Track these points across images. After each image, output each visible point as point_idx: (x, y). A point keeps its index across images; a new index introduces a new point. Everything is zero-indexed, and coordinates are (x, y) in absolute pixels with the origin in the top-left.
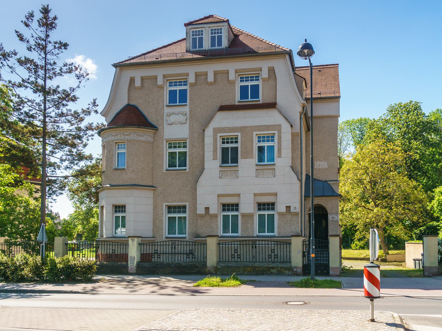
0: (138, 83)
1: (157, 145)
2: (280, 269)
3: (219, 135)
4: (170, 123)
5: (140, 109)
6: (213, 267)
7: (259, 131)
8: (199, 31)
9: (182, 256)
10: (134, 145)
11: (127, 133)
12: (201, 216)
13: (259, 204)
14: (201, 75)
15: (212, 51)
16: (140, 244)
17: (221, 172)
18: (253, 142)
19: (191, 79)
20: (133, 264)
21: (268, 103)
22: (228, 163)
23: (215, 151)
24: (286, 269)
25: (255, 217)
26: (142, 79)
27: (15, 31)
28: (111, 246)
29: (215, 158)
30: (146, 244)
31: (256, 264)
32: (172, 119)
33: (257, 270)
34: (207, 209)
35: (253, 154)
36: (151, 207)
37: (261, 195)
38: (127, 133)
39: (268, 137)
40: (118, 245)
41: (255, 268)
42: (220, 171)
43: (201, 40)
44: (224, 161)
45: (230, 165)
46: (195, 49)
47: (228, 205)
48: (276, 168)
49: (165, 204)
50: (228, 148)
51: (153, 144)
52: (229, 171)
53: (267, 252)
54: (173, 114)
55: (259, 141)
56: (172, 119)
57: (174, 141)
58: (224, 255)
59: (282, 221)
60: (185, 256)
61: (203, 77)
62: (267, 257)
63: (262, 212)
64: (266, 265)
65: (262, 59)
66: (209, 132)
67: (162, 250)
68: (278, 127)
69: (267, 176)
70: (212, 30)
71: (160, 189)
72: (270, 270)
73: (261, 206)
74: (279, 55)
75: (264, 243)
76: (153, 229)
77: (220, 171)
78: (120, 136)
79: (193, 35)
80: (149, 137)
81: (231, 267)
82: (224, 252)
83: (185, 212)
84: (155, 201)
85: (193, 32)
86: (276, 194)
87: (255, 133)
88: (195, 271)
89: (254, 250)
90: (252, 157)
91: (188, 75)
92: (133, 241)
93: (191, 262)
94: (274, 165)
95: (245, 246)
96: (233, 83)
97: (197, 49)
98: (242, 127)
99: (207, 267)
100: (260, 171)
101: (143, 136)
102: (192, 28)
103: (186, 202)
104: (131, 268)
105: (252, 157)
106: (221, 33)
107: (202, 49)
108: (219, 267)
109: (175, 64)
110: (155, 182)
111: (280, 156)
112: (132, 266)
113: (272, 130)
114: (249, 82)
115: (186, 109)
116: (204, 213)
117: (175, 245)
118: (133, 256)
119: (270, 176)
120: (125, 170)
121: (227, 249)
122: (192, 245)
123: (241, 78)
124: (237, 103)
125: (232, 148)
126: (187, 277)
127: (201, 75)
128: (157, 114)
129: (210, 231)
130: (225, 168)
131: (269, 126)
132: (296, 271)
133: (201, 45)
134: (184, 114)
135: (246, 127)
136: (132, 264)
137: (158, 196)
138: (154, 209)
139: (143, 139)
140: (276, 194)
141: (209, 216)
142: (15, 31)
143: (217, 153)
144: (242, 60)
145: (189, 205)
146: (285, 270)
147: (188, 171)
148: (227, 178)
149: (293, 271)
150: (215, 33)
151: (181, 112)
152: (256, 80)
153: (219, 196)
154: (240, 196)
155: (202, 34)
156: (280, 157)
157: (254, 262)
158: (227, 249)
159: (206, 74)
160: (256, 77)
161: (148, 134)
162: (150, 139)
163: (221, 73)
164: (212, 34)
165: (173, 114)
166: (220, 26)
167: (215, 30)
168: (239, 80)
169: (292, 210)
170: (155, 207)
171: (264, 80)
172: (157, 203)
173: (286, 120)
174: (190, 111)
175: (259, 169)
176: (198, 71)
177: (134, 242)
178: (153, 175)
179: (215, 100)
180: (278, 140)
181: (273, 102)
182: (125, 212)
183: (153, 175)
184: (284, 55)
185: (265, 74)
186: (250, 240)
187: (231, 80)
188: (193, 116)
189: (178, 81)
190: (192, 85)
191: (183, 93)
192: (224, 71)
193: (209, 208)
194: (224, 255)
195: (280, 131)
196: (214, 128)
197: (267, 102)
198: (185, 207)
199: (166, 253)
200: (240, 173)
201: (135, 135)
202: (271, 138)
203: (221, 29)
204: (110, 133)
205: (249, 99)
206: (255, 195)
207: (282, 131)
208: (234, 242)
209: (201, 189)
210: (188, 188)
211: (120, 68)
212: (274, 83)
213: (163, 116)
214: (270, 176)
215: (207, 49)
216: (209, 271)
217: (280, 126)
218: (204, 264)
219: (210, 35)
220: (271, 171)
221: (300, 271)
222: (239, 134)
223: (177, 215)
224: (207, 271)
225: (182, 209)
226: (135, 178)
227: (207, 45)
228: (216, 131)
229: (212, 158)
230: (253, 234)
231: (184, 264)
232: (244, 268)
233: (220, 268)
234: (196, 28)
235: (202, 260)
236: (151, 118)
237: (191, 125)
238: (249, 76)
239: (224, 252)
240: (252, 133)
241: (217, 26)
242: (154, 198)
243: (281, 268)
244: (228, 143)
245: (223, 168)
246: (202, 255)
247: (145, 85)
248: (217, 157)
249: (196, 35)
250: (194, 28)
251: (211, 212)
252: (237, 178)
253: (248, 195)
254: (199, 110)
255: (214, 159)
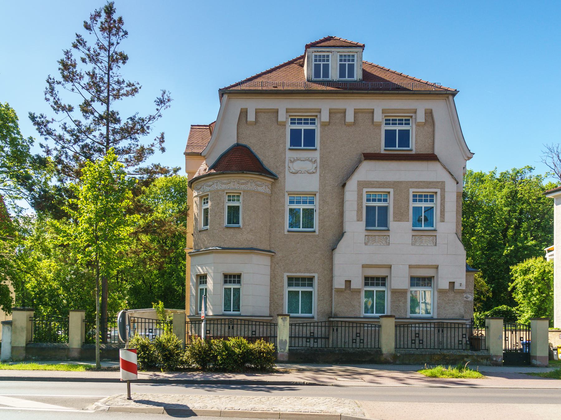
0: (251, 117)
1: (276, 199)
2: (476, 358)
3: (365, 190)
4: (294, 171)
5: (254, 151)
6: (391, 354)
7: (417, 188)
8: (324, 56)
9: (297, 339)
10: (252, 197)
11: (243, 181)
12: (339, 291)
13: (366, 278)
14: (335, 113)
15: (342, 83)
16: (291, 325)
17: (366, 237)
18: (409, 201)
19: (325, 117)
20: (285, 349)
21: (423, 154)
22: (375, 226)
23: (359, 210)
24: (483, 357)
25: (362, 293)
26: (257, 112)
27: (77, 35)
28: (250, 327)
29: (359, 220)
30: (403, 326)
31: (445, 352)
32: (297, 166)
33: (447, 359)
34: (348, 282)
35: (408, 216)
36: (268, 278)
37: (416, 268)
38: (243, 181)
39: (426, 196)
40: (360, 327)
41: (445, 356)
42: (366, 236)
43: (326, 67)
44: (369, 223)
45: (377, 228)
46: (318, 79)
47: (372, 278)
48: (438, 235)
49: (286, 275)
50: (374, 207)
51: (270, 196)
52: (377, 236)
53: (409, 335)
54: (298, 159)
55: (415, 201)
56: (297, 166)
57: (297, 194)
58: (369, 340)
59: (443, 299)
60: (304, 340)
61: (339, 115)
62: (351, 341)
63: (228, 286)
64: (458, 353)
65: (417, 98)
66: (352, 186)
67: (319, 333)
68: (441, 185)
69: (379, 244)
70: (341, 56)
71: (279, 255)
72: (463, 359)
73: (369, 281)
74: (441, 96)
75: (421, 325)
76: (270, 306)
77: (366, 236)
78: (234, 185)
79: (316, 61)
80: (267, 187)
81: (413, 354)
82: (369, 337)
83: (311, 285)
84: (273, 270)
85: (316, 56)
86: (437, 267)
87: (411, 190)
88: (367, 360)
89: (335, 334)
90: (407, 220)
91: (320, 112)
92: (284, 320)
93: (358, 348)
94: (435, 230)
95: (351, 328)
96: (283, 125)
97: (321, 79)
98: (395, 182)
99: (382, 354)
100: (417, 237)
101: (262, 186)
102: (315, 52)
103: (314, 272)
104: (281, 355)
105: (407, 220)
106: (353, 60)
107: (328, 79)
108: (398, 355)
109: (304, 96)
110: (273, 246)
111: (442, 221)
112: (283, 352)
113: (433, 188)
114: (404, 125)
115: (316, 155)
116: (343, 287)
117: (234, 324)
118: (284, 339)
119: (429, 245)
120: (241, 229)
121: (373, 332)
122: (314, 326)
123: (291, 119)
124: (383, 152)
125: (379, 207)
126: (376, 366)
127: (335, 113)
128: (276, 159)
129: (351, 309)
130: (372, 231)
131: (430, 183)
132: (496, 361)
133: (326, 74)
134: (313, 160)
135: (401, 182)
136: (282, 350)
137: (277, 264)
138: (271, 281)
139: (260, 189)
140: (437, 267)
141: (349, 292)
142: (77, 35)
143: (362, 213)
144: (392, 98)
145: (318, 277)
146: (482, 359)
147: (317, 233)
148: (374, 244)
149: (493, 360)
150: (345, 61)
151: (309, 158)
152: (311, 123)
153: (364, 266)
154: (391, 268)
155: (328, 61)
156: (443, 221)
157: (441, 349)
158: (373, 332)
159: (344, 112)
160: (406, 120)
161: (266, 184)
162: (268, 191)
163: (362, 113)
164: (341, 60)
165: (298, 159)
166: (353, 52)
167: (345, 56)
168: (290, 121)
169: (457, 287)
170: (273, 277)
171: (418, 125)
172: (276, 273)
173: (451, 176)
174: (321, 158)
175: (416, 236)
176: (334, 107)
177: (286, 322)
178: (270, 237)
179: (354, 146)
180: (441, 200)
181: (429, 153)
182: (206, 283)
183: (270, 237)
184: (447, 96)
185: (421, 117)
186: (239, 319)
187: (377, 122)
188: (324, 165)
189: (296, 118)
190: (324, 125)
191: (310, 135)
192: (368, 109)
193: (350, 281)
194: (369, 340)
195: (443, 190)
196: (358, 181)
197: (422, 153)
198: (311, 279)
199: (299, 337)
200: (392, 239)
201: (253, 184)
202: (430, 197)
203: (353, 56)
204: (218, 179)
205: (397, 148)
206: (411, 267)
207: (446, 190)
208: (415, 324)
209: (339, 257)
210: (317, 255)
211: (228, 96)
212: (431, 130)
213: (284, 162)
214: (429, 245)
215: (335, 80)
216: (386, 359)
217: (443, 183)
218: (379, 351)
219: (339, 63)
220: (431, 238)
221: (501, 360)
222: (391, 191)
223: (300, 289)
224: (382, 359)
225: (309, 281)
226: (252, 240)
227: (334, 75)
228: (362, 185)
229: (355, 218)
230: (406, 315)
231: (351, 350)
232: (431, 356)
233: (400, 356)
234: (320, 52)
235: (377, 347)
236: (268, 161)
237: (322, 175)
238: (398, 118)
239: (369, 337)
240: (408, 190)
241: (348, 52)
242: (271, 266)
243: (478, 356)
244: (374, 200)
245: (369, 231)
246: (343, 340)
247: (260, 120)
248: (362, 217)
249: (320, 61)
250: (318, 52)
251: (353, 286)
252: (387, 245)
253: (401, 266)
254: (333, 157)
255: (358, 220)
